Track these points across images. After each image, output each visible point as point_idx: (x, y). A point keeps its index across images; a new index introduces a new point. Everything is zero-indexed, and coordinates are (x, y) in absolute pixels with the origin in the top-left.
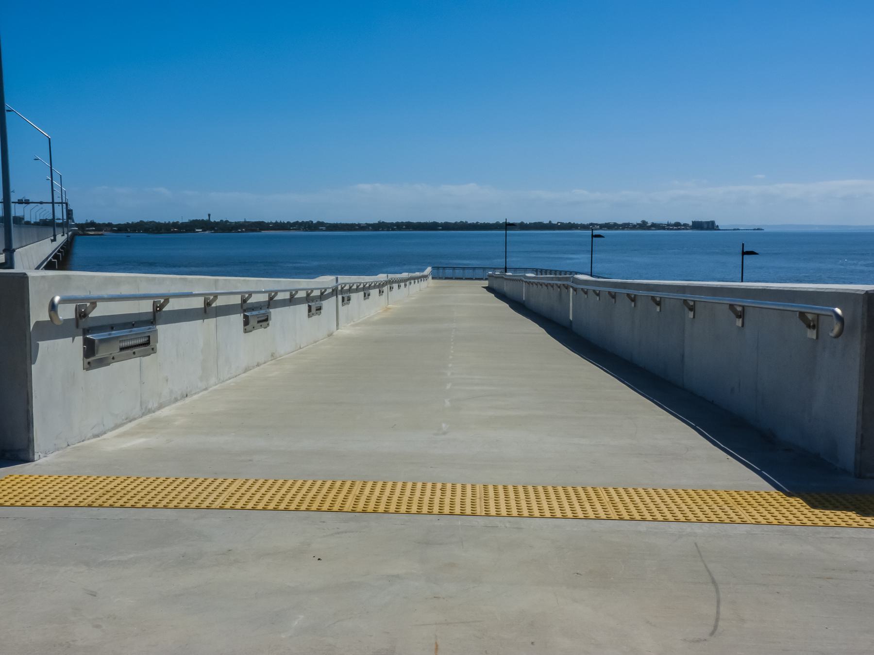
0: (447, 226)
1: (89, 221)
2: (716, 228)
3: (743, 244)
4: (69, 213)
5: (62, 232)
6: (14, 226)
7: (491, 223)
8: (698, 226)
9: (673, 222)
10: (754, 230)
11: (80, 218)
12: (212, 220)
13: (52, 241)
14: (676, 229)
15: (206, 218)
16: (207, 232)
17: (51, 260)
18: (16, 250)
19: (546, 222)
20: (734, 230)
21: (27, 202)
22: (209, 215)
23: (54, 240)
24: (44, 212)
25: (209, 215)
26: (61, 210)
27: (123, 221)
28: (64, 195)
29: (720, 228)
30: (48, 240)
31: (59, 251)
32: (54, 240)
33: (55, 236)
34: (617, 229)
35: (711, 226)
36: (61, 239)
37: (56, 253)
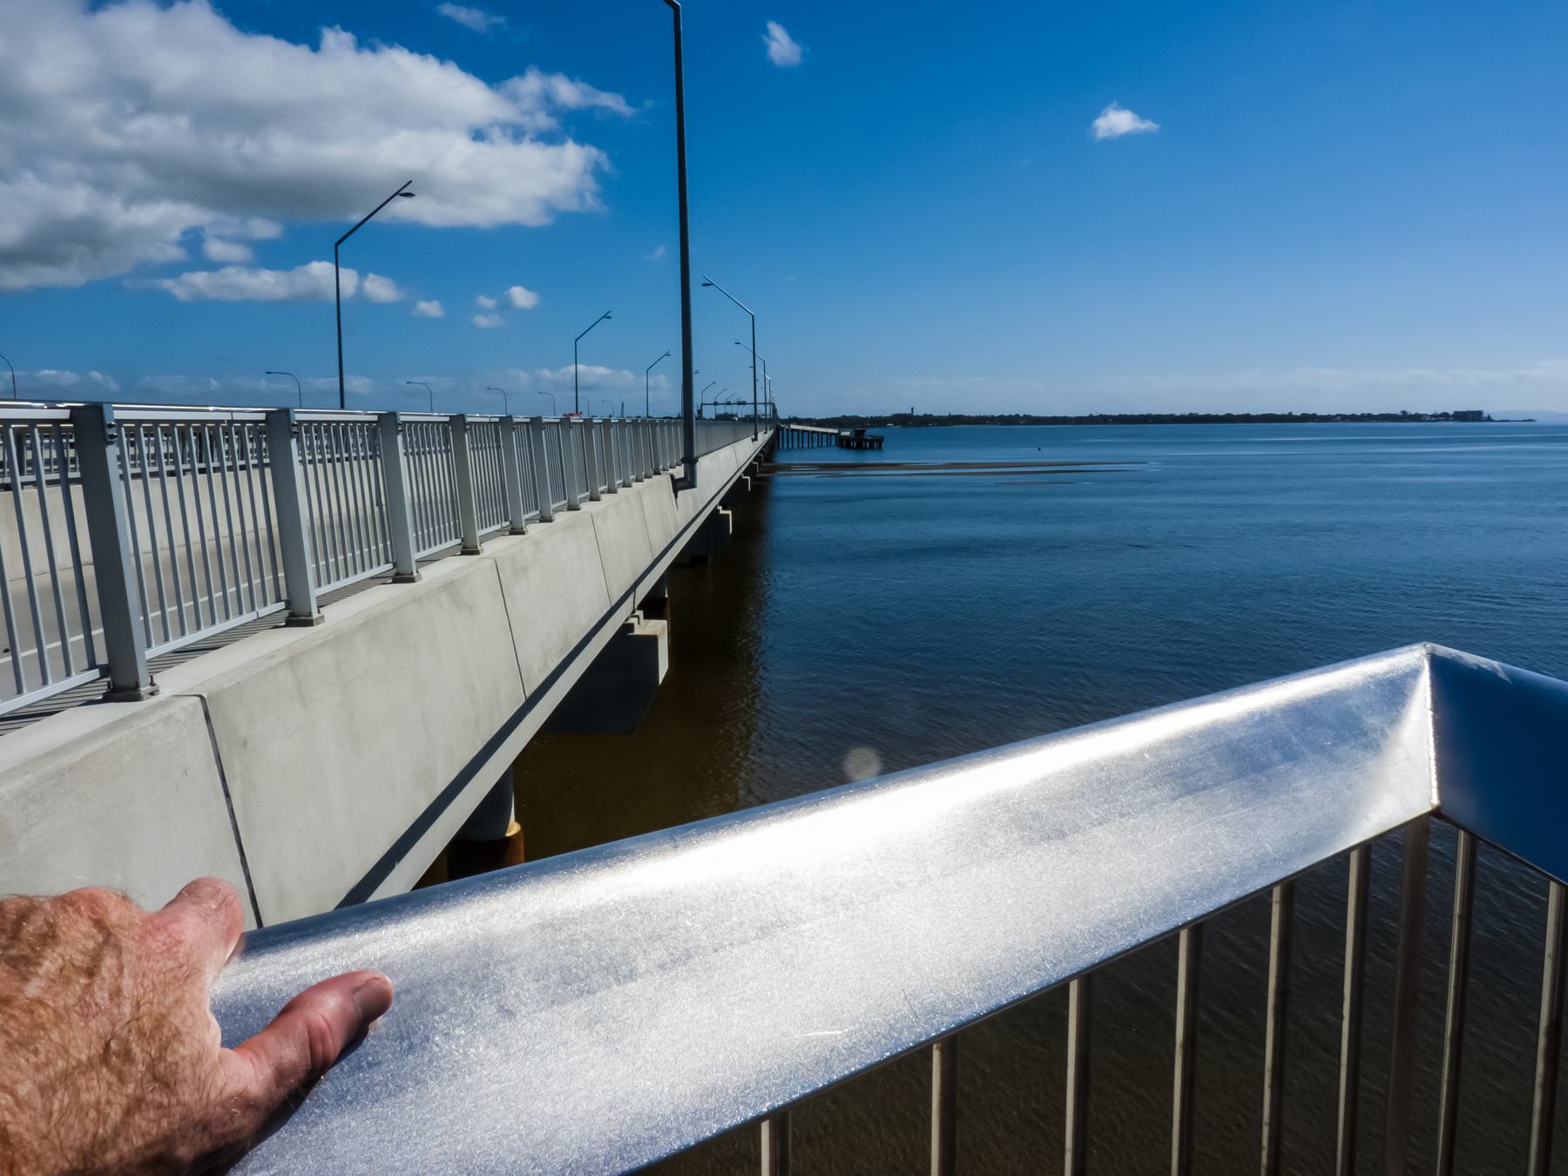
0: (1247, 418)
1: (792, 417)
2: (1492, 421)
3: (410, 182)
4: (775, 411)
5: (754, 431)
6: (697, 424)
7: (973, 415)
8: (1461, 416)
9: (1440, 412)
10: (1524, 421)
11: (782, 415)
12: (915, 414)
13: (678, 485)
14: (1434, 421)
15: (908, 412)
16: (898, 427)
17: (741, 476)
18: (700, 460)
19: (1086, 414)
20: (1524, 421)
21: (744, 403)
22: (912, 409)
23: (766, 433)
24: (747, 411)
25: (912, 409)
26: (384, 201)
27: (824, 417)
28: (767, 386)
29: (1494, 419)
30: (749, 440)
31: (761, 452)
32: (755, 439)
33: (756, 435)
34: (1447, 420)
35: (1476, 416)
36: (764, 437)
37: (751, 463)
